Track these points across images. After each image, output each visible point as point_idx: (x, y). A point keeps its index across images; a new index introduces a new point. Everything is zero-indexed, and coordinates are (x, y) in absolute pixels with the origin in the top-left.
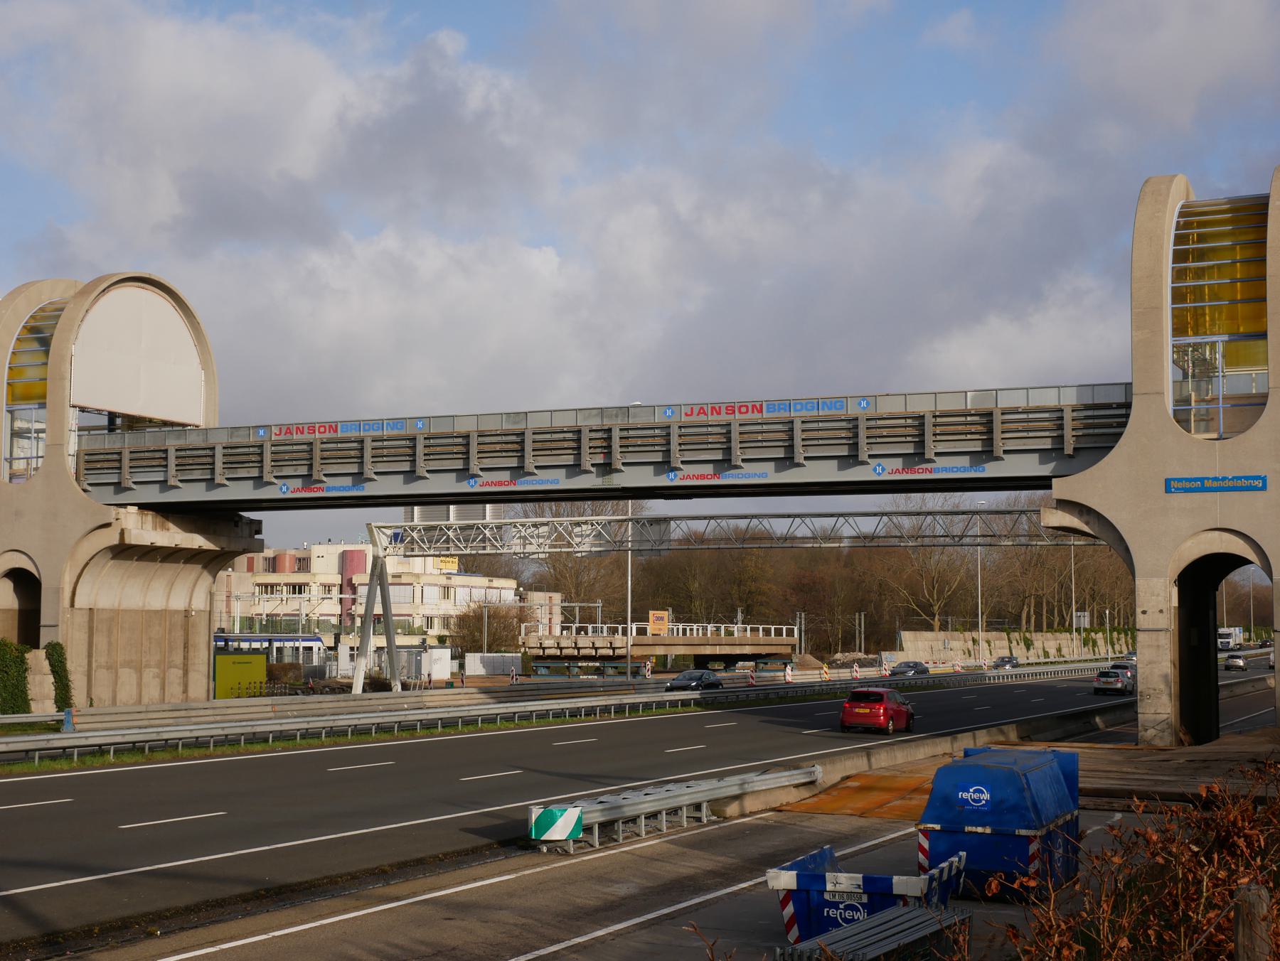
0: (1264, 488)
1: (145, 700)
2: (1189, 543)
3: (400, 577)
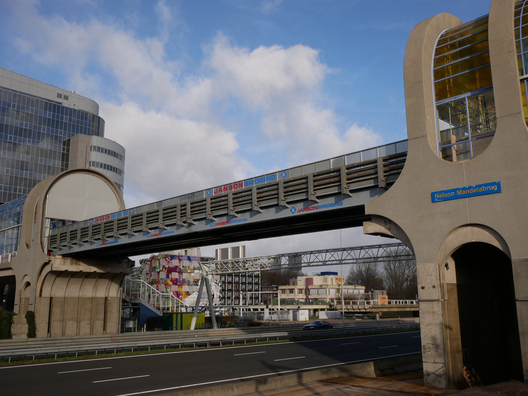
0: (499, 191)
1: (82, 333)
2: (451, 237)
3: (322, 286)
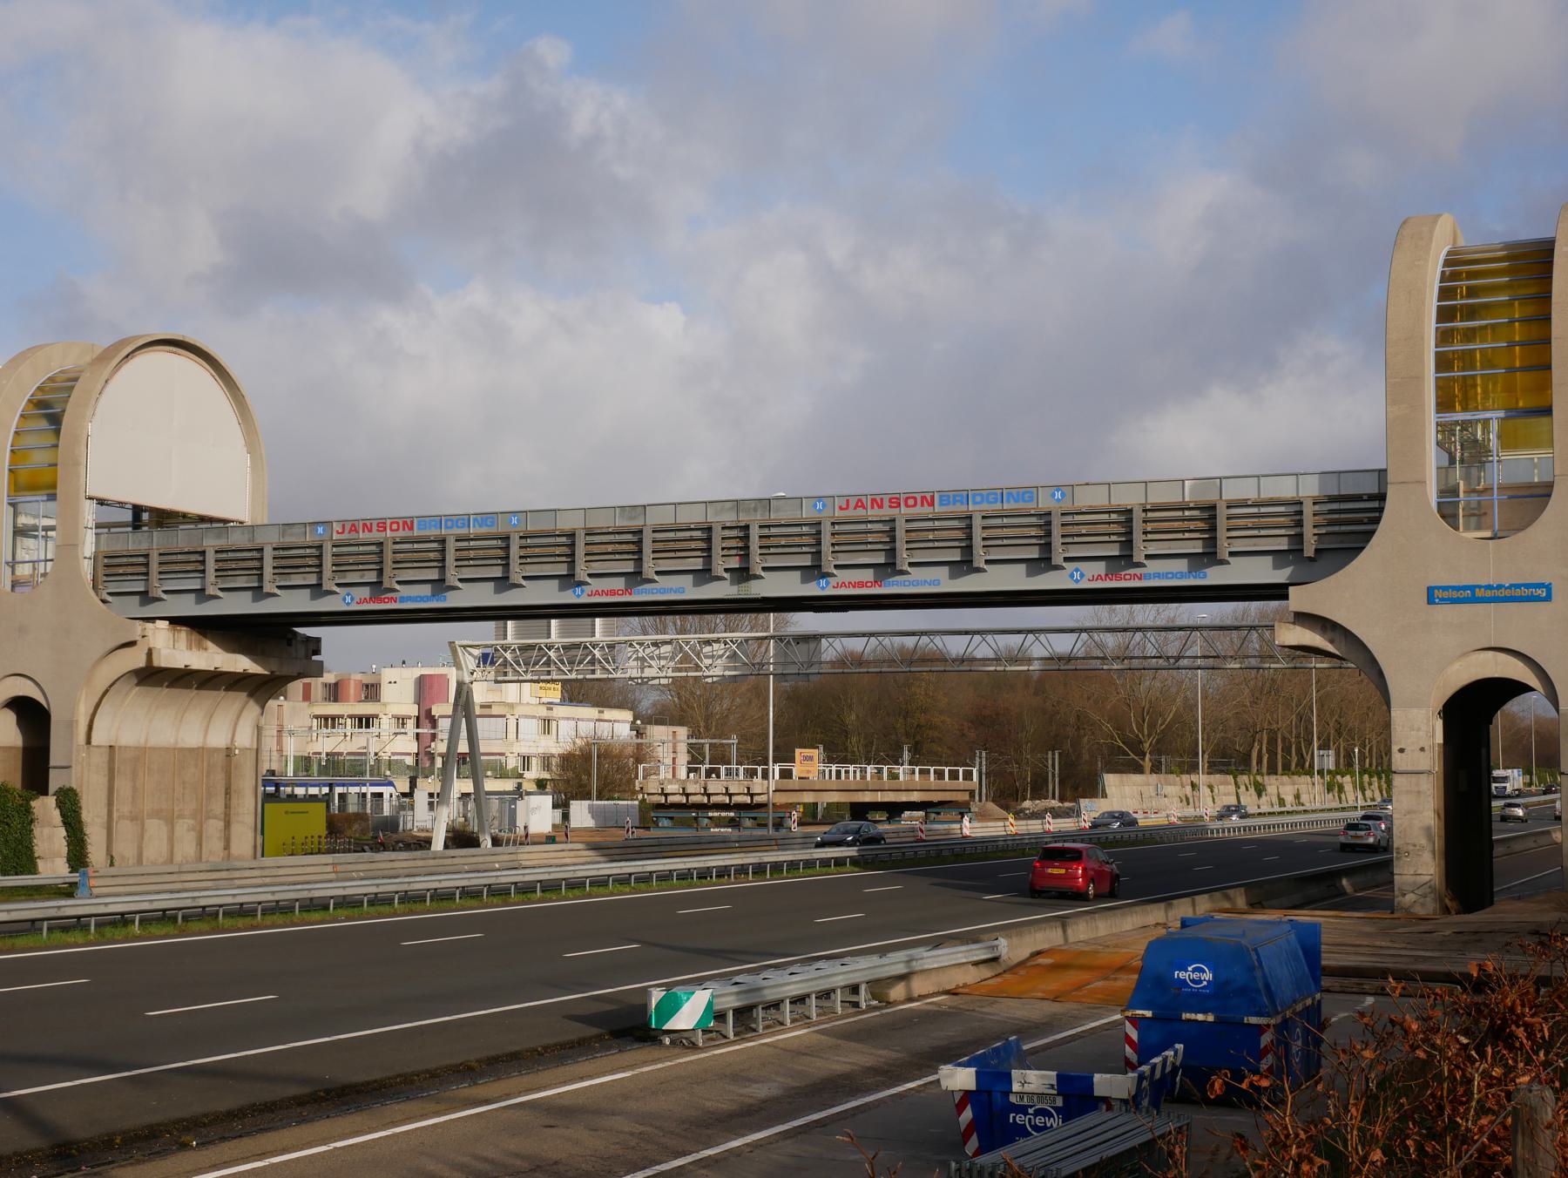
0: (1548, 598)
1: (178, 858)
2: (1456, 666)
3: (490, 707)
